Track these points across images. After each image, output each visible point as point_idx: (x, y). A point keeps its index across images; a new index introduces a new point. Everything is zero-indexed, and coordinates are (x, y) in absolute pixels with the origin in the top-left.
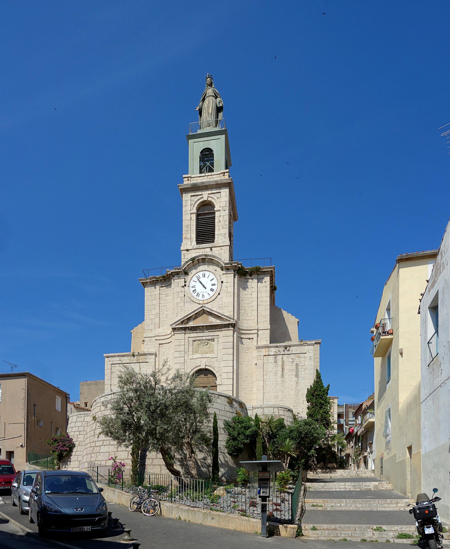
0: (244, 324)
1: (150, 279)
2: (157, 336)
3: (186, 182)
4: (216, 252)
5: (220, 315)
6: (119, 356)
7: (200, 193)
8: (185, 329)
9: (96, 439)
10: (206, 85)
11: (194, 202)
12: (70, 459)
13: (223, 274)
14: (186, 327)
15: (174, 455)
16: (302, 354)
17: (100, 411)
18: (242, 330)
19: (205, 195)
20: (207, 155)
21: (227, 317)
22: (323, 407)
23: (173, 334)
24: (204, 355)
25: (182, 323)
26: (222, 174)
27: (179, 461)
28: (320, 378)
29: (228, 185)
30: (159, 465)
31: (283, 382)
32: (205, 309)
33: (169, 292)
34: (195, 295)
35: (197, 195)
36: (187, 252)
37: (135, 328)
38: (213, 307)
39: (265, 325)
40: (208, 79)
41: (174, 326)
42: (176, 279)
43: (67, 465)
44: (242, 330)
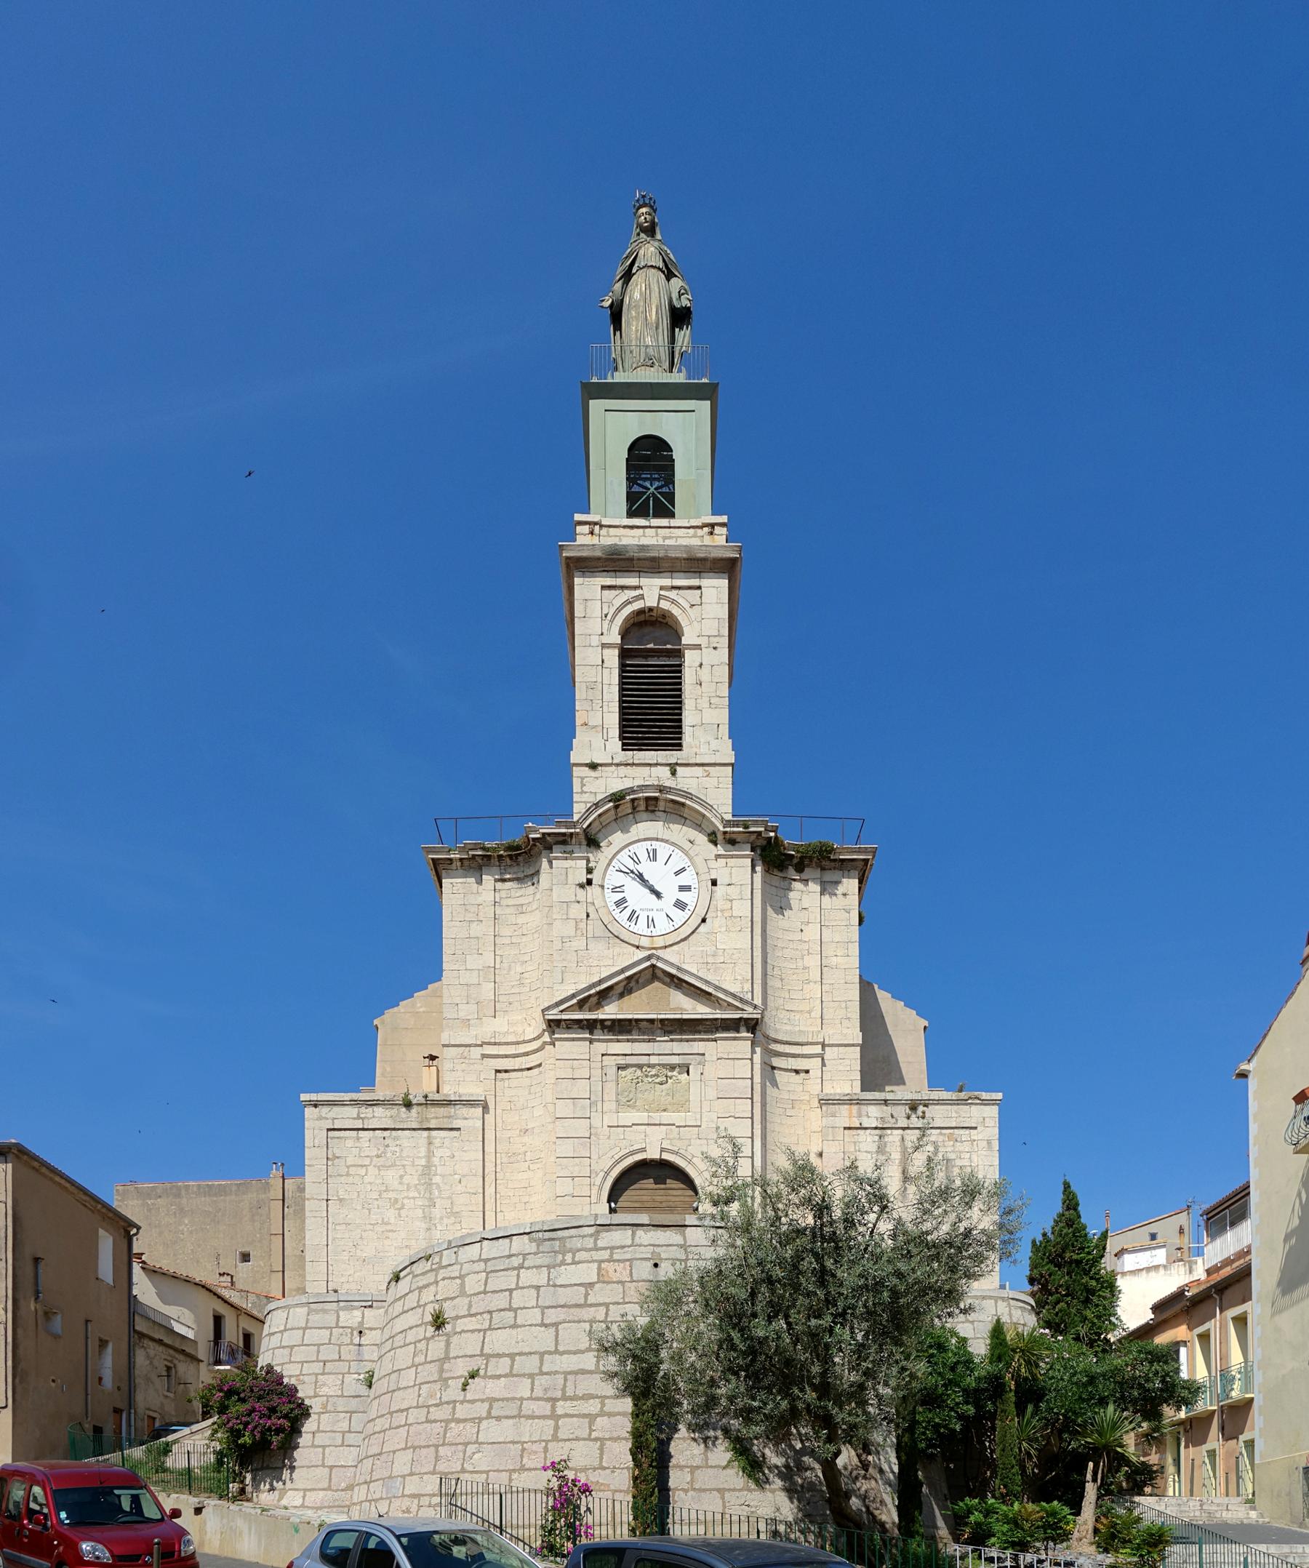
0: (779, 1026)
1: (462, 850)
2: (489, 1044)
4: (688, 780)
5: (710, 990)
6: (355, 1103)
8: (591, 1026)
9: (454, 1391)
10: (635, 231)
12: (292, 1459)
13: (718, 856)
14: (595, 1021)
15: (763, 1455)
16: (962, 1132)
18: (776, 1041)
19: (652, 591)
20: (649, 459)
21: (734, 996)
22: (1095, 1299)
23: (546, 1038)
24: (656, 1117)
25: (581, 1005)
26: (706, 529)
27: (781, 1476)
28: (1075, 1209)
29: (727, 567)
30: (718, 1490)
32: (659, 965)
35: (623, 588)
39: (845, 1031)
40: (644, 210)
41: (554, 1014)
42: (556, 858)
43: (279, 1479)
44: (776, 1041)
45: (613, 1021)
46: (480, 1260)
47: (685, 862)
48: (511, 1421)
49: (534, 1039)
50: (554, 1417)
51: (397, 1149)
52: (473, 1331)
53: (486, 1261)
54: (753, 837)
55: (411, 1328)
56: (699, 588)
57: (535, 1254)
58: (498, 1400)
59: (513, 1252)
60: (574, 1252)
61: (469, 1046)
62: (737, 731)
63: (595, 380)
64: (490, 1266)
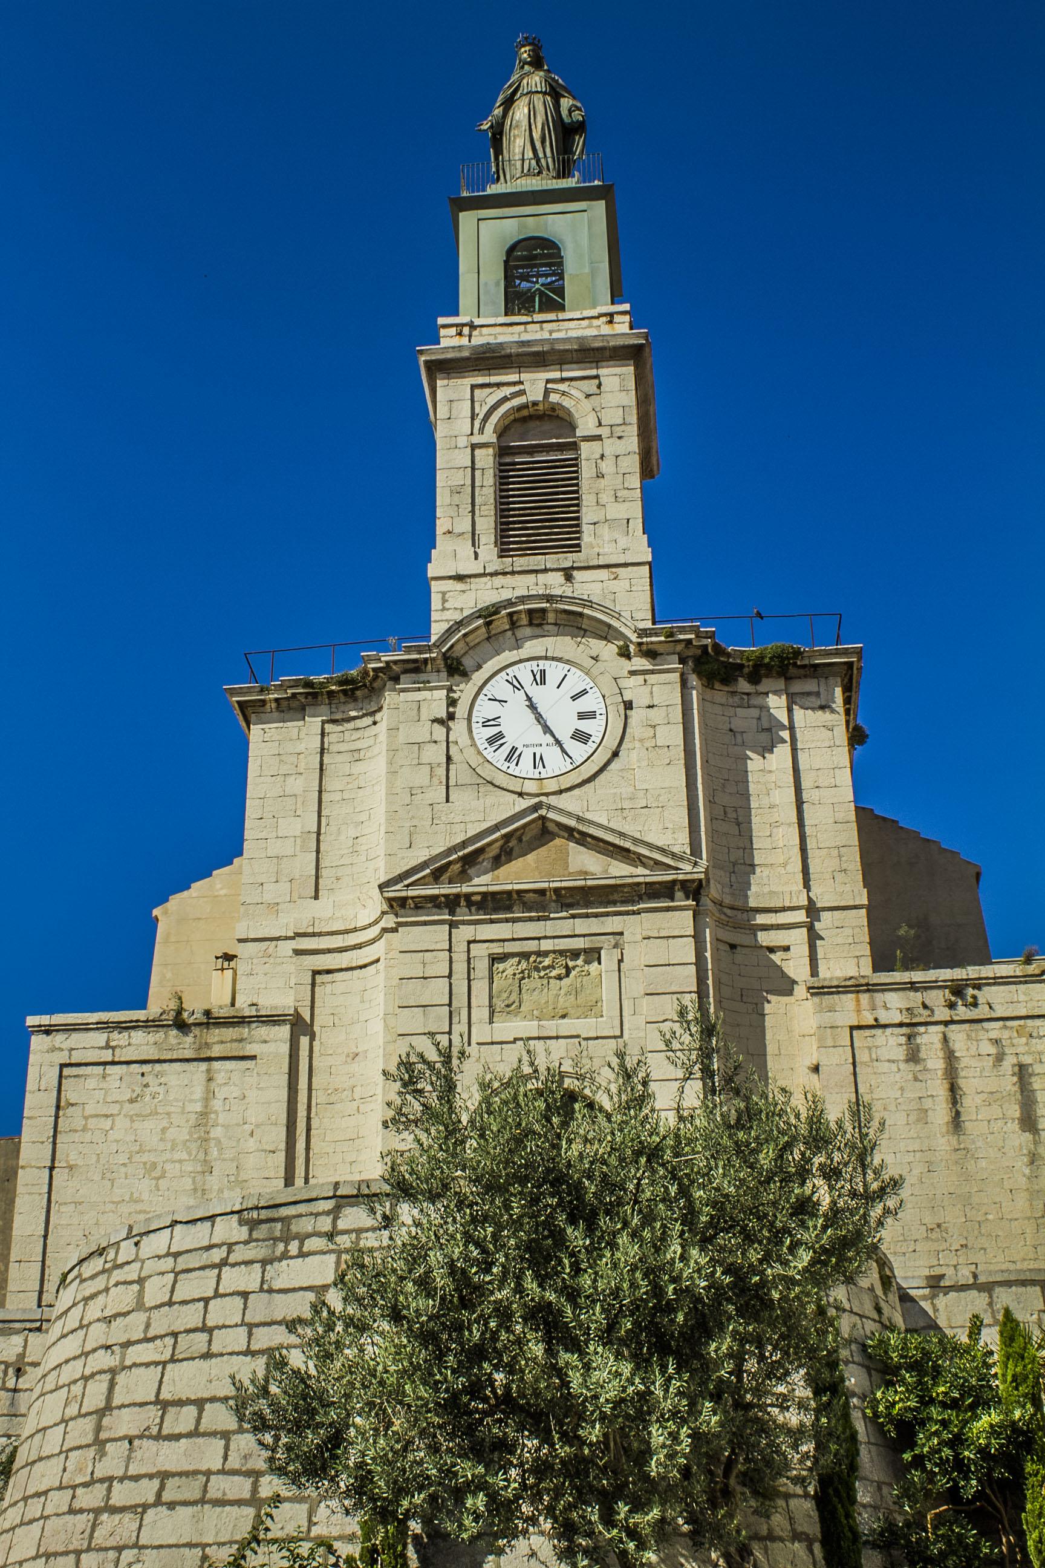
2: (304, 935)
3: (449, 340)
4: (589, 586)
5: (627, 845)
7: (514, 377)
11: (485, 409)
13: (633, 673)
14: (458, 896)
17: (140, 1306)
19: (534, 385)
21: (662, 850)
24: (552, 1027)
25: (437, 875)
26: (604, 319)
29: (632, 354)
31: (963, 1153)
32: (551, 815)
33: (371, 742)
34: (498, 757)
35: (498, 385)
36: (459, 586)
37: (175, 901)
38: (594, 807)
41: (397, 891)
45: (485, 895)
46: (168, 1254)
47: (586, 683)
48: (190, 1510)
49: (370, 925)
50: (254, 1501)
51: (161, 1090)
52: (147, 1365)
53: (177, 1255)
54: (680, 647)
55: (67, 1362)
56: (597, 377)
57: (246, 1243)
58: (174, 1475)
59: (215, 1241)
60: (302, 1238)
61: (278, 939)
62: (653, 525)
63: (465, 194)
64: (183, 1263)
